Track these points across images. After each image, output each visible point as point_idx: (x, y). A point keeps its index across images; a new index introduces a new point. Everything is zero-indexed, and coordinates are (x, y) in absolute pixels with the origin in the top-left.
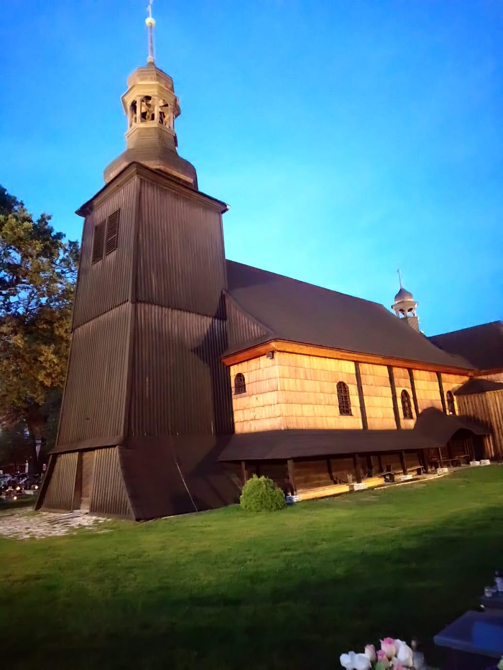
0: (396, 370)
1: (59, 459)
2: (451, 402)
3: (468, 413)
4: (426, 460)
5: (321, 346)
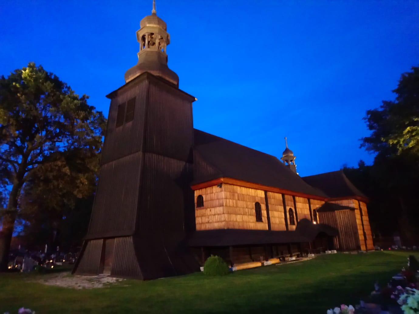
0: (286, 196)
1: (89, 243)
2: (315, 215)
3: (325, 223)
4: (302, 250)
5: (248, 182)
